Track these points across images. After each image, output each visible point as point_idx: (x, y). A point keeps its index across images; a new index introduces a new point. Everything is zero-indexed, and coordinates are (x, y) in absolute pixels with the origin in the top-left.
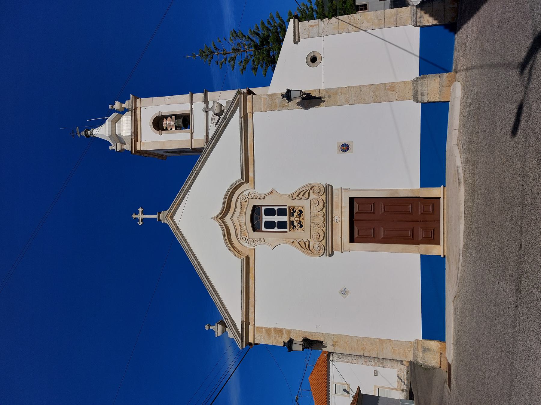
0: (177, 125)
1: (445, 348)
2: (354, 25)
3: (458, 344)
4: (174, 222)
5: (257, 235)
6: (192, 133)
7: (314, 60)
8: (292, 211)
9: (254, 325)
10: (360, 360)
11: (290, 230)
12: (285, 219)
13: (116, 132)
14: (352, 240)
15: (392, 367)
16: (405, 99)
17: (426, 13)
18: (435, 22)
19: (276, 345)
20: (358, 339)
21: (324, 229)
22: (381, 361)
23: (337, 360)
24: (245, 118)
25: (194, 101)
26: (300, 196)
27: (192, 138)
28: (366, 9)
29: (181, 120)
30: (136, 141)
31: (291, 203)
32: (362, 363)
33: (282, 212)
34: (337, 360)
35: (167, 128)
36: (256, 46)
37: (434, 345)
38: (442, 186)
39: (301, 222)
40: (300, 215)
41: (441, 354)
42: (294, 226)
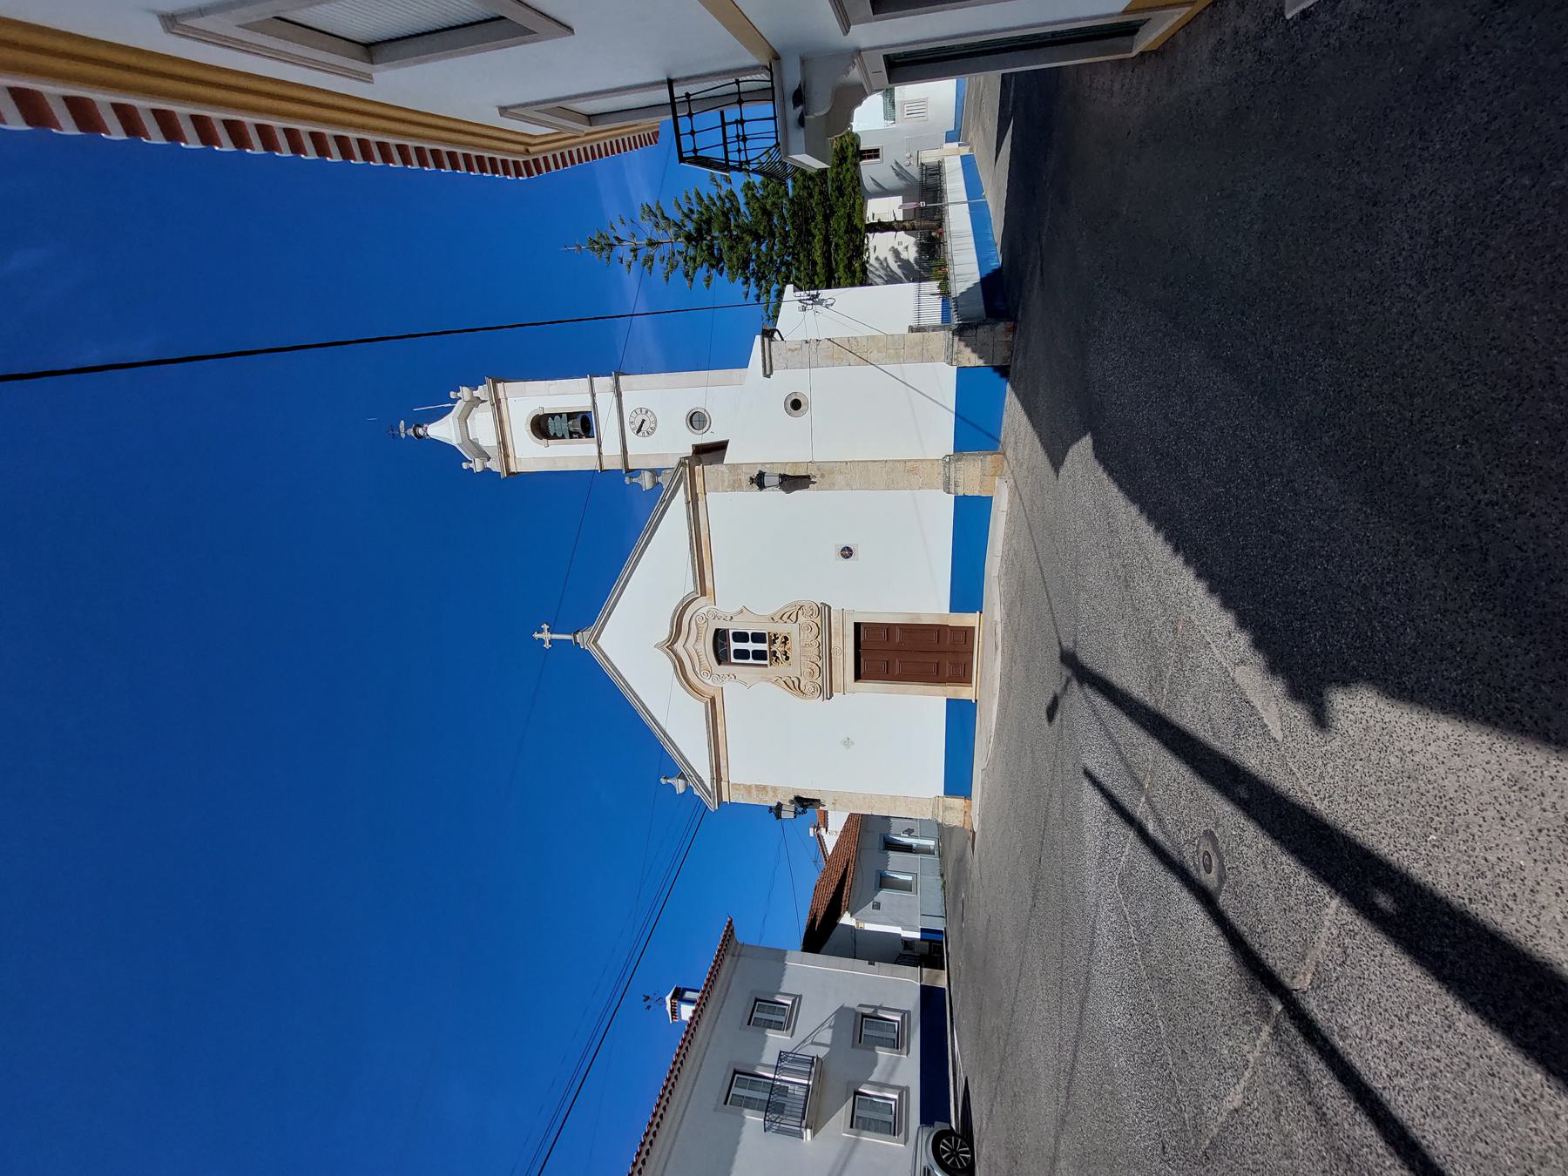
0: (571, 429)
1: (970, 806)
2: (858, 354)
3: (985, 810)
4: (599, 648)
5: (724, 669)
6: (599, 446)
7: (796, 405)
8: (773, 638)
9: (729, 782)
11: (771, 664)
13: (468, 436)
14: (858, 677)
16: (931, 486)
17: (967, 346)
18: (981, 363)
21: (820, 664)
24: (693, 502)
25: (596, 390)
26: (785, 618)
27: (600, 453)
28: (877, 156)
29: (578, 422)
30: (506, 456)
33: (758, 638)
35: (555, 434)
36: (689, 238)
37: (958, 802)
38: (978, 613)
39: (786, 652)
40: (785, 643)
41: (965, 812)
42: (777, 658)
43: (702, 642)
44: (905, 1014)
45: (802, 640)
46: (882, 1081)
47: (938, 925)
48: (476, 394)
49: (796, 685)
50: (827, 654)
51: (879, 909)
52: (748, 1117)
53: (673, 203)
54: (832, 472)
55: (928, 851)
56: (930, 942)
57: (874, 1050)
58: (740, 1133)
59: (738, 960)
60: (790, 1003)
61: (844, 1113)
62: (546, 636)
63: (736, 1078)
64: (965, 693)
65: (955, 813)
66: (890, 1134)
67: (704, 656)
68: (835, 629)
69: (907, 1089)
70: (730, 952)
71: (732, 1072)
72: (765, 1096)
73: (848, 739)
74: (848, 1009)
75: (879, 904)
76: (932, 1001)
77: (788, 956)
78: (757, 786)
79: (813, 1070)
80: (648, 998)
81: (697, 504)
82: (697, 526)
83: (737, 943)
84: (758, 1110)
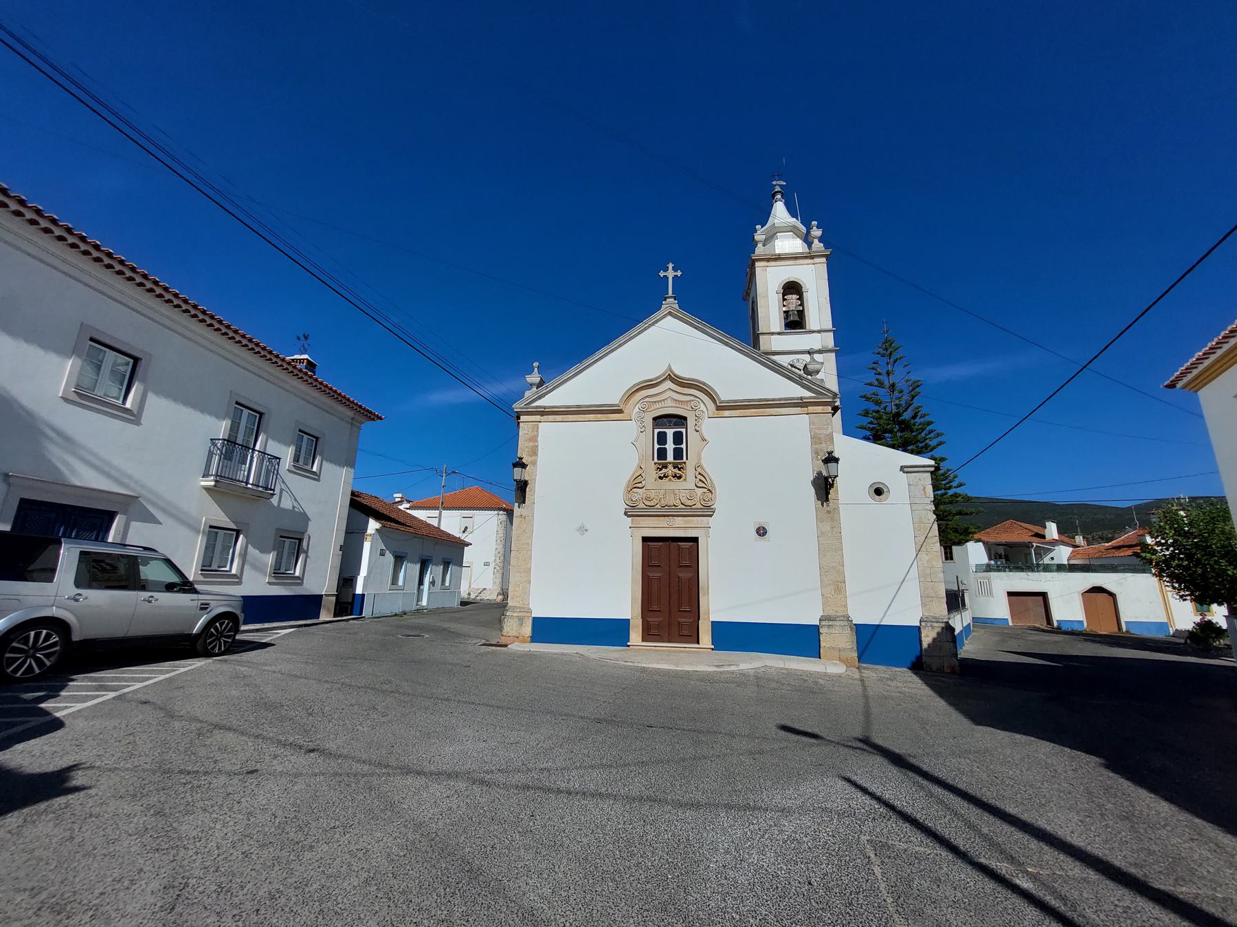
0: (791, 313)
1: (523, 641)
4: (665, 316)
6: (779, 334)
7: (879, 492)
8: (680, 467)
9: (540, 422)
11: (655, 464)
12: (670, 457)
14: (645, 539)
15: (495, 583)
17: (938, 633)
18: (925, 645)
21: (658, 506)
24: (801, 403)
27: (773, 334)
29: (797, 318)
30: (768, 260)
33: (678, 454)
35: (786, 300)
37: (527, 630)
38: (713, 647)
39: (666, 477)
41: (518, 637)
42: (661, 470)
44: (300, 580)
45: (683, 489)
46: (248, 557)
47: (366, 612)
48: (816, 241)
49: (637, 485)
50: (668, 512)
51: (381, 555)
52: (224, 423)
53: (919, 405)
54: (833, 520)
55: (419, 599)
56: (352, 604)
57: (274, 550)
58: (210, 414)
59: (348, 423)
60: (314, 469)
61: (223, 519)
62: (671, 274)
63: (256, 414)
64: (635, 636)
65: (516, 629)
66: (202, 566)
67: (660, 406)
68: (692, 521)
69: (239, 583)
70: (356, 417)
71: (261, 410)
72: (239, 441)
73: (586, 530)
74: (307, 525)
75: (384, 556)
76: (305, 607)
77: (349, 469)
78: (537, 447)
79: (260, 489)
80: (306, 338)
81: (798, 407)
82: (756, 407)
83: (361, 423)
84: (230, 434)
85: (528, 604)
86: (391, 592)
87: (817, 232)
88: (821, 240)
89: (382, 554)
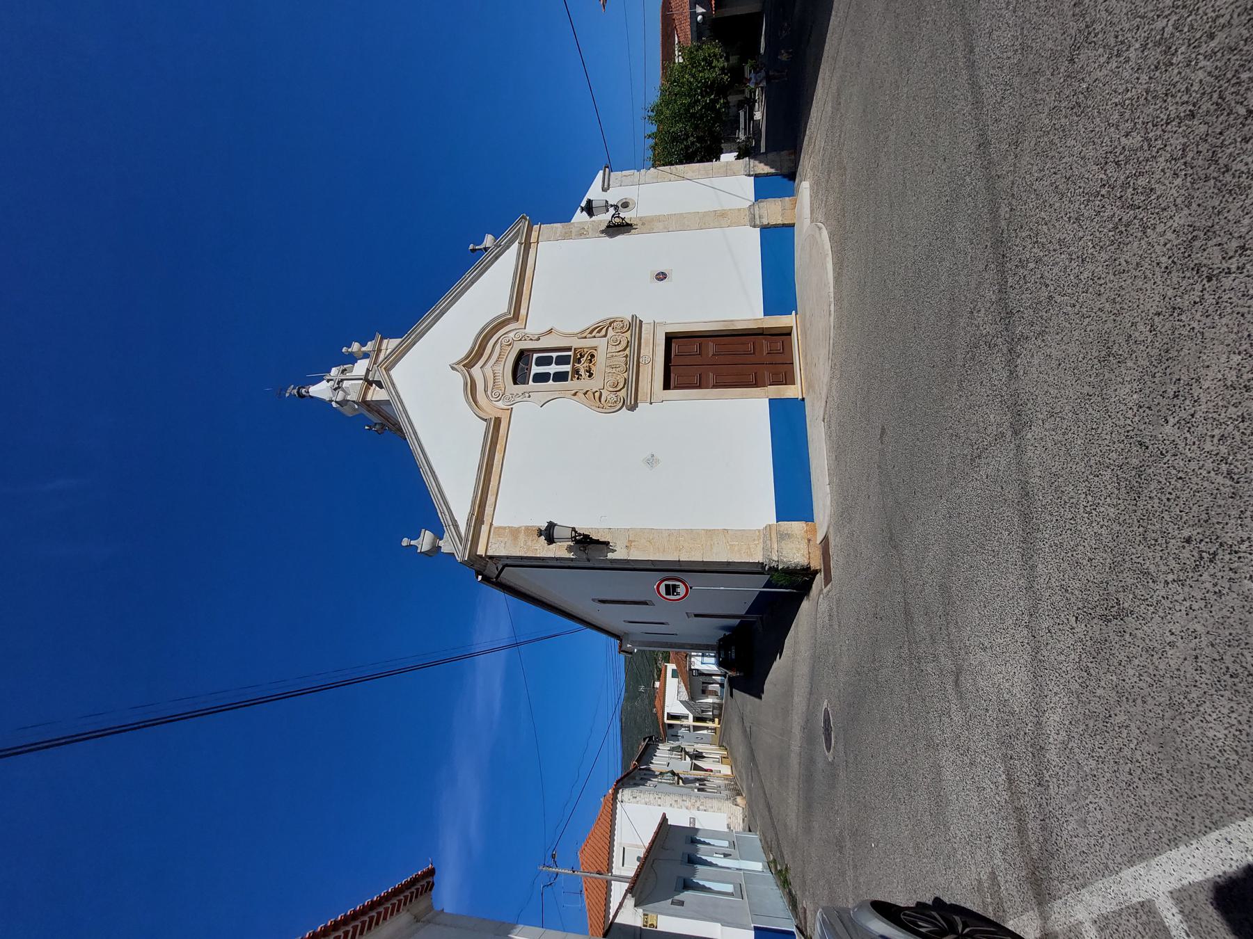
4: (390, 377)
5: (520, 388)
9: (491, 524)
10: (668, 798)
12: (566, 368)
15: (719, 809)
19: (525, 555)
20: (670, 533)
22: (702, 801)
23: (629, 800)
24: (527, 246)
31: (576, 343)
32: (671, 805)
34: (629, 800)
37: (797, 527)
38: (794, 312)
39: (590, 368)
41: (809, 540)
43: (503, 363)
48: (364, 349)
50: (635, 365)
83: (430, 908)
85: (759, 531)
86: (745, 896)
87: (355, 347)
88: (364, 344)
89: (681, 903)
